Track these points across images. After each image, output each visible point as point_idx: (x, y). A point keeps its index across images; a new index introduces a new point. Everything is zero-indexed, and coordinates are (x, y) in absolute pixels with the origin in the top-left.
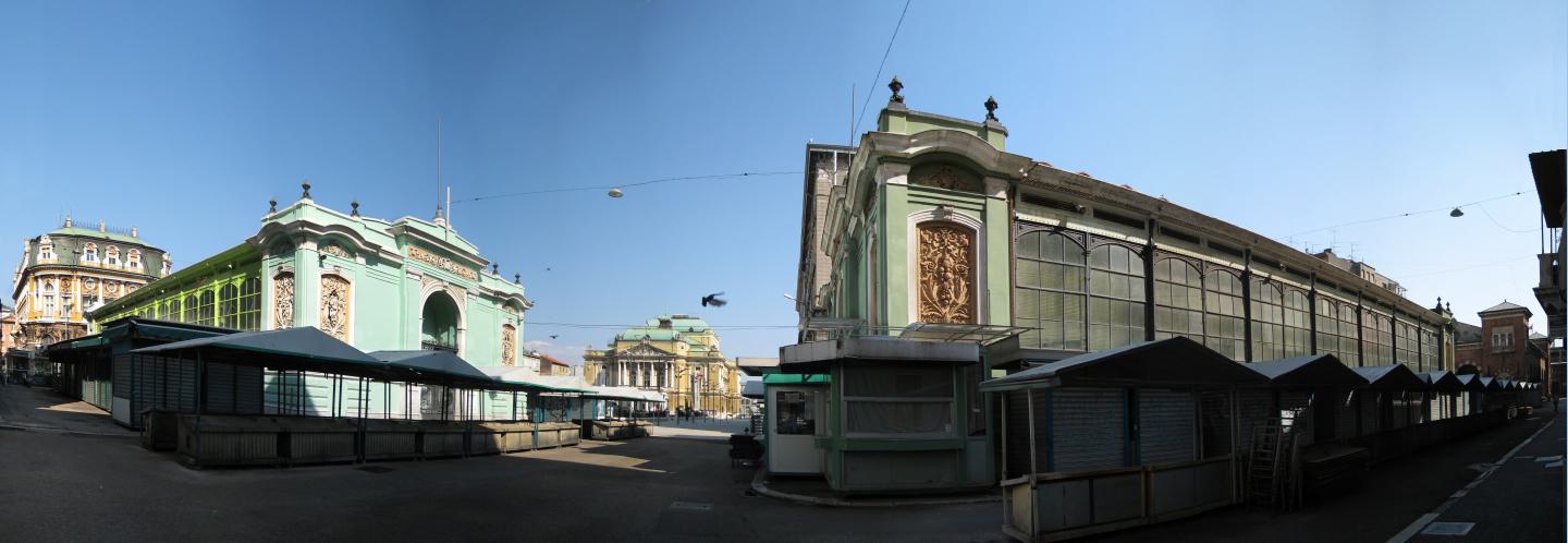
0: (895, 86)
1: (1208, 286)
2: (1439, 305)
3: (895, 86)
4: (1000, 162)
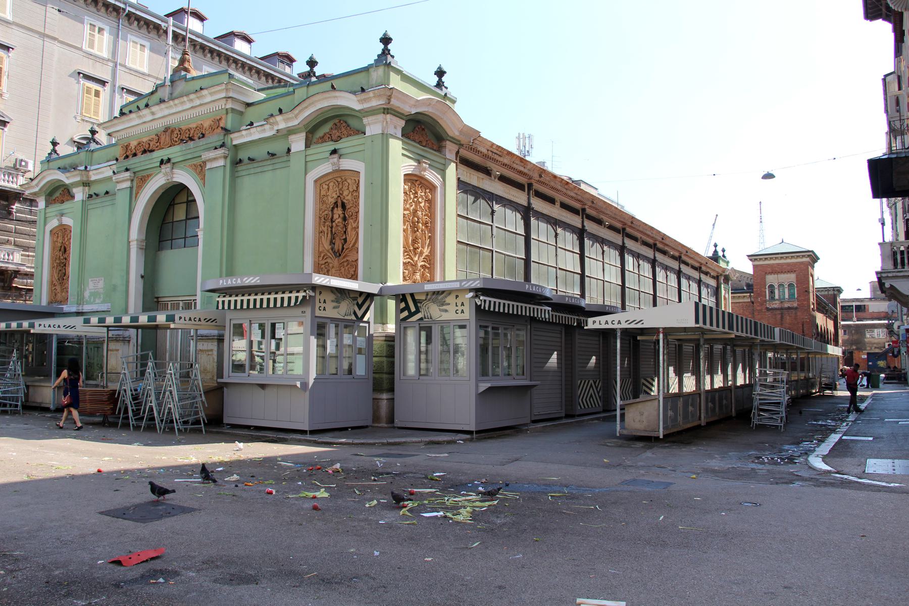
0: (386, 40)
1: (559, 245)
2: (716, 251)
3: (386, 40)
4: (461, 132)
